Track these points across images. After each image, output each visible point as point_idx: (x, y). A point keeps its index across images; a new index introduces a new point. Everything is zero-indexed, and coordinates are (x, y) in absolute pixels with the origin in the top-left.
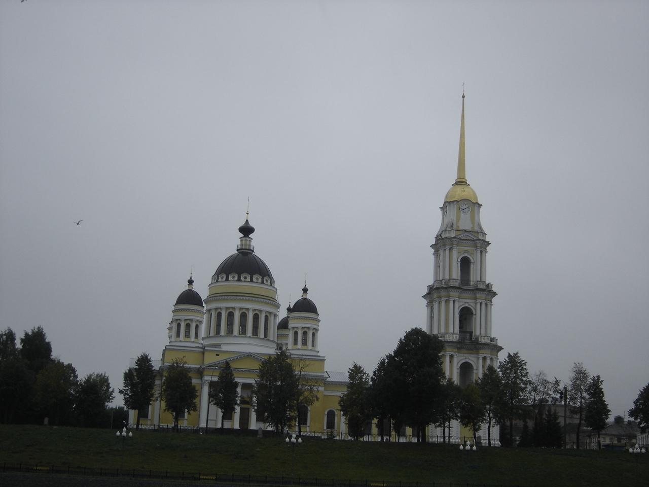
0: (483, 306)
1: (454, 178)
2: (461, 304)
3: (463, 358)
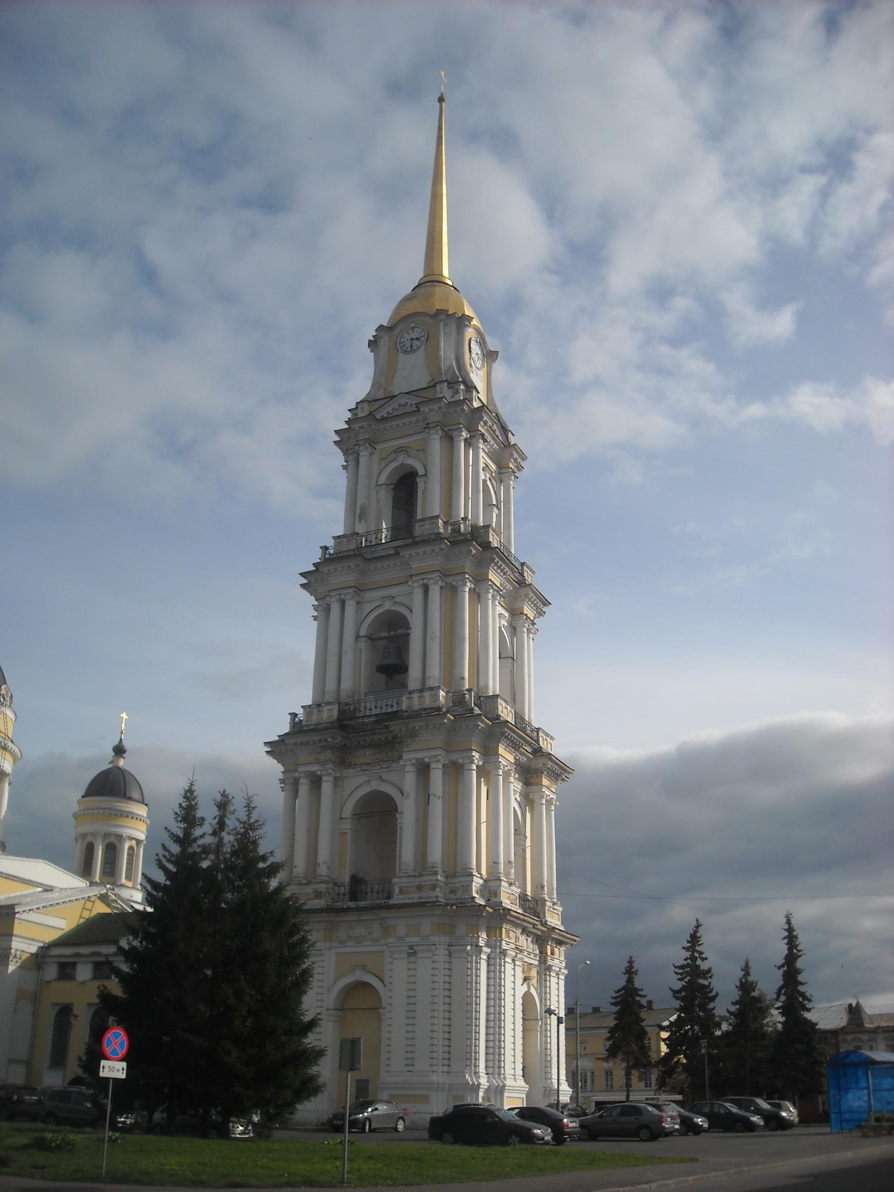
0: (435, 593)
1: (417, 274)
2: (367, 608)
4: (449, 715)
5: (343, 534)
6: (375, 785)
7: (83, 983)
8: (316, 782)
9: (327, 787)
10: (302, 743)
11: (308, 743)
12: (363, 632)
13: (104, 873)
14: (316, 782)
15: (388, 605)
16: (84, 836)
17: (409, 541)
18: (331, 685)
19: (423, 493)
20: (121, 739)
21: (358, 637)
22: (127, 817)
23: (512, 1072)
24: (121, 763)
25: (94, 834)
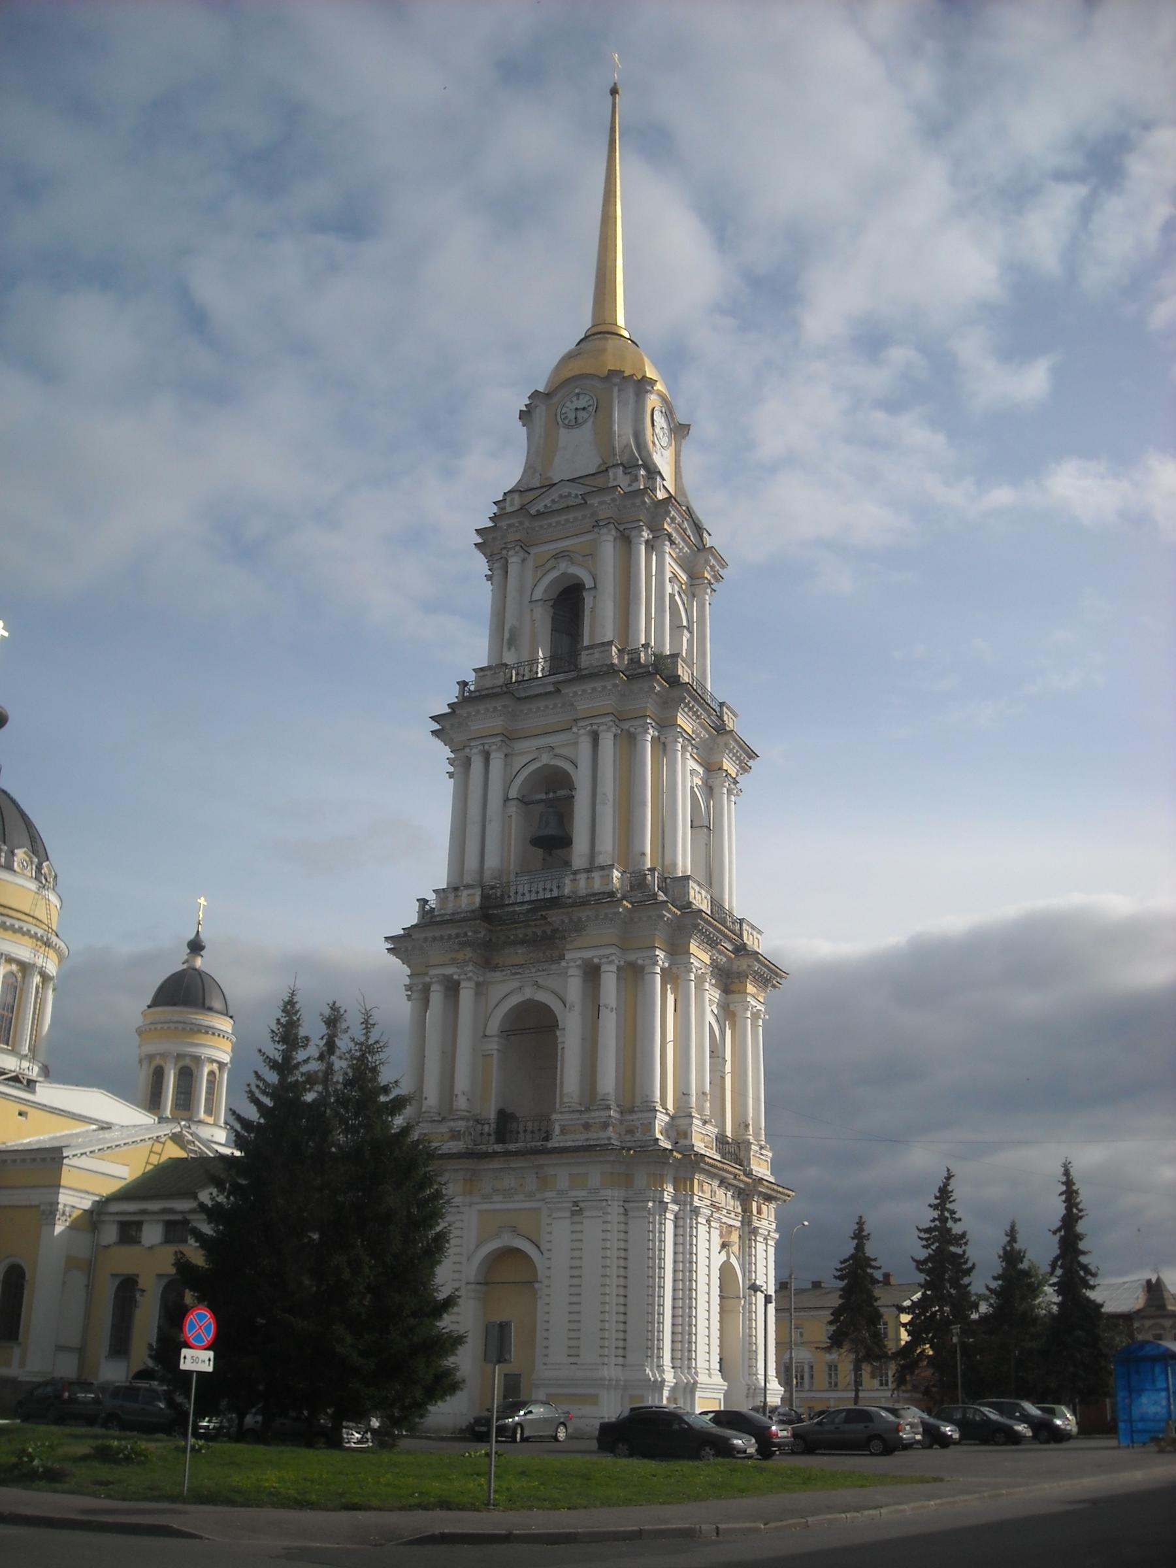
2: (519, 762)
3: (513, 984)
4: (625, 902)
5: (486, 665)
6: (529, 993)
7: (151, 1248)
8: (452, 989)
9: (466, 995)
10: (434, 939)
11: (442, 938)
12: (513, 793)
13: (176, 1105)
14: (452, 989)
15: (545, 759)
16: (151, 1057)
17: (573, 674)
18: (471, 863)
19: (591, 612)
20: (198, 931)
21: (506, 800)
22: (207, 1033)
23: (706, 1365)
24: (199, 963)
25: (164, 1056)
